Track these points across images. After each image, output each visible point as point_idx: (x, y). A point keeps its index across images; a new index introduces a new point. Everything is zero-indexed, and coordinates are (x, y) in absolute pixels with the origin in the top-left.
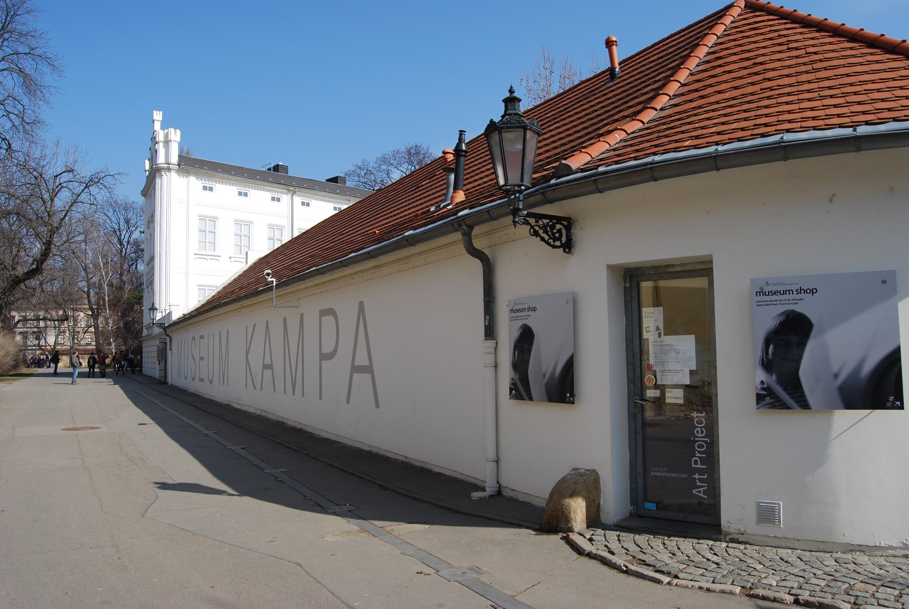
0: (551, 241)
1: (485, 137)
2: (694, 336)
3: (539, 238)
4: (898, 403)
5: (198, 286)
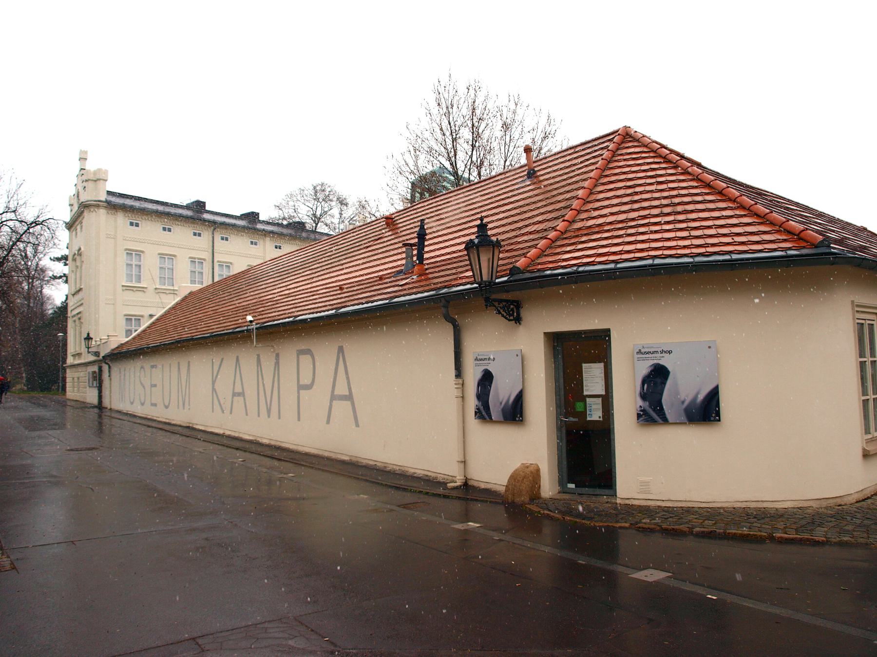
0: (507, 316)
1: (466, 249)
2: (584, 365)
3: (500, 315)
4: (718, 418)
5: (125, 315)
